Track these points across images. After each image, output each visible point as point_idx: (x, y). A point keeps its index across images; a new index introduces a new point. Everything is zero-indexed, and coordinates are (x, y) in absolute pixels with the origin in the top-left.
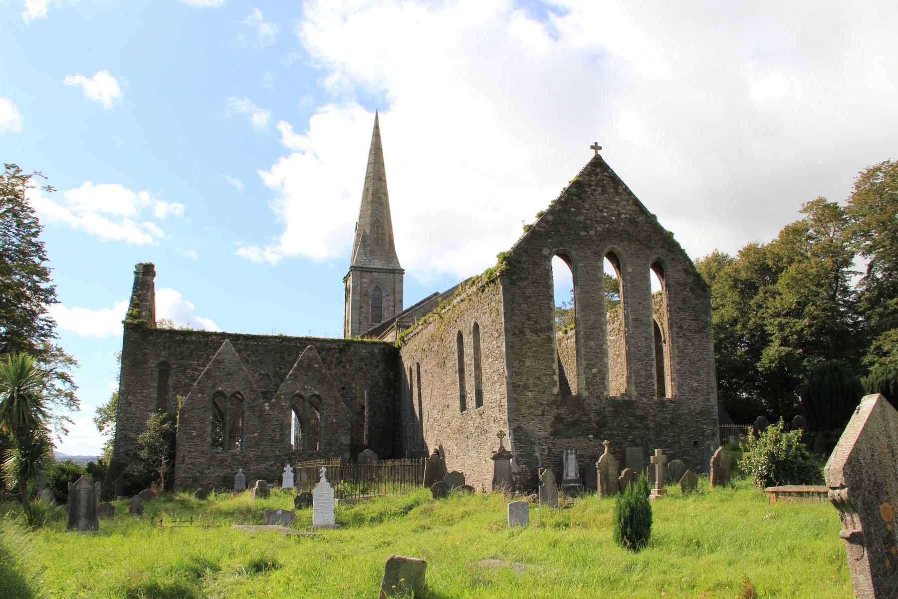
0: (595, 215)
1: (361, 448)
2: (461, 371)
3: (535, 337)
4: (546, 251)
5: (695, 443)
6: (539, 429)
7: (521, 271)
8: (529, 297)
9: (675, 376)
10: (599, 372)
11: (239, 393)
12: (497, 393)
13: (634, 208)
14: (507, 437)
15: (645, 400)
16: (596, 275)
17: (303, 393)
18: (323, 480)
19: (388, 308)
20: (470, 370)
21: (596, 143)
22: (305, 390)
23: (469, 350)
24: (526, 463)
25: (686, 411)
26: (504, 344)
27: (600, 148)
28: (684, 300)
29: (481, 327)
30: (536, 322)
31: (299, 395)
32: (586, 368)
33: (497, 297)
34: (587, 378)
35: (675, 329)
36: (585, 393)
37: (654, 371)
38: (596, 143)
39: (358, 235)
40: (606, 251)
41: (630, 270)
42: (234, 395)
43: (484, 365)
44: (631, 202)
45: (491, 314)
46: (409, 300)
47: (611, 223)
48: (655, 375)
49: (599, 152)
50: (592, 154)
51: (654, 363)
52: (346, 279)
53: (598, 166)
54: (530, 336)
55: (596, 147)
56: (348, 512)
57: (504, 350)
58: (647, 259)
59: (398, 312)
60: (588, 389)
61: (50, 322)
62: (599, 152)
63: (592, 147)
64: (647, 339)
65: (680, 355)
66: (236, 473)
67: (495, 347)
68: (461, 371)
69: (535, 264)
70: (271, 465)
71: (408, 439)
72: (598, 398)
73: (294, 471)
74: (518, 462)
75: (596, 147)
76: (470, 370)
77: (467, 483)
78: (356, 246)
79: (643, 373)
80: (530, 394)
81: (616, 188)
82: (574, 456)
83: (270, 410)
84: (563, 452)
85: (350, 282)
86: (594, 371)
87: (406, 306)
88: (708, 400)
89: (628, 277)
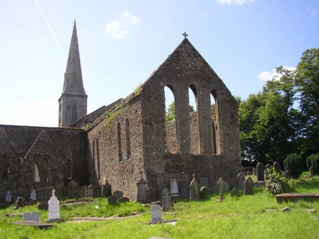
0: (186, 67)
1: (70, 181)
2: (119, 142)
3: (156, 125)
4: (162, 84)
5: (231, 175)
6: (158, 169)
7: (149, 94)
8: (154, 105)
9: (222, 144)
10: (187, 142)
11: (8, 154)
12: (138, 153)
13: (203, 64)
14: (143, 174)
15: (208, 155)
16: (185, 96)
17: (40, 154)
18: (54, 196)
19: (80, 114)
20: (124, 142)
21: (185, 33)
22: (41, 152)
23: (123, 132)
24: (153, 186)
25: (227, 160)
26: (141, 129)
27: (187, 35)
28: (226, 108)
29: (130, 121)
30: (157, 118)
31: (38, 155)
32: (181, 140)
33: (138, 106)
34: (181, 145)
35: (222, 122)
36: (180, 152)
37: (212, 142)
38: (185, 33)
39: (66, 79)
40: (190, 84)
41: (201, 93)
42: (5, 155)
43: (132, 139)
44: (202, 61)
45: (136, 113)
46: (90, 110)
47: (193, 71)
48: (213, 144)
49: (187, 37)
50: (183, 38)
51: (212, 137)
52: (60, 100)
53: (186, 41)
54: (155, 125)
55: (185, 35)
56: (67, 214)
57: (141, 131)
58: (209, 88)
59: (84, 116)
60: (182, 150)
61: (286, 199)
62: (187, 37)
63: (183, 35)
64: (209, 126)
65: (225, 135)
66: (6, 194)
67: (137, 129)
68: (119, 142)
69: (156, 89)
70: (24, 190)
71: (92, 176)
72: (187, 154)
73: (36, 192)
74: (149, 185)
75: (185, 35)
76: (124, 142)
77: (124, 196)
78: (65, 84)
79: (207, 142)
80: (154, 152)
81: (194, 54)
82: (175, 183)
83: (24, 162)
84: (170, 180)
85: (61, 102)
86: (185, 141)
87: (89, 112)
88: (237, 155)
89: (200, 97)
